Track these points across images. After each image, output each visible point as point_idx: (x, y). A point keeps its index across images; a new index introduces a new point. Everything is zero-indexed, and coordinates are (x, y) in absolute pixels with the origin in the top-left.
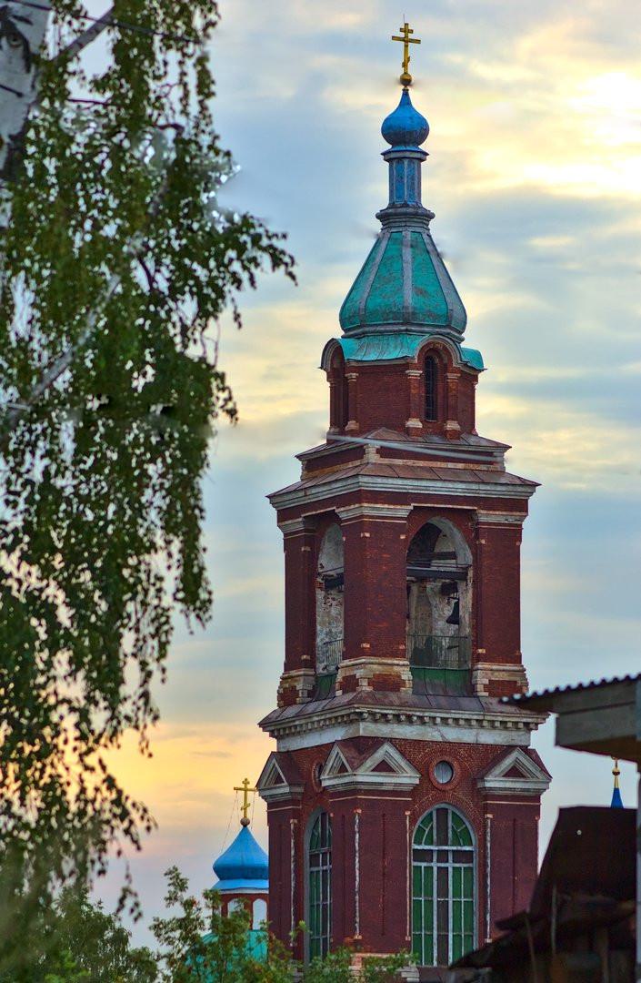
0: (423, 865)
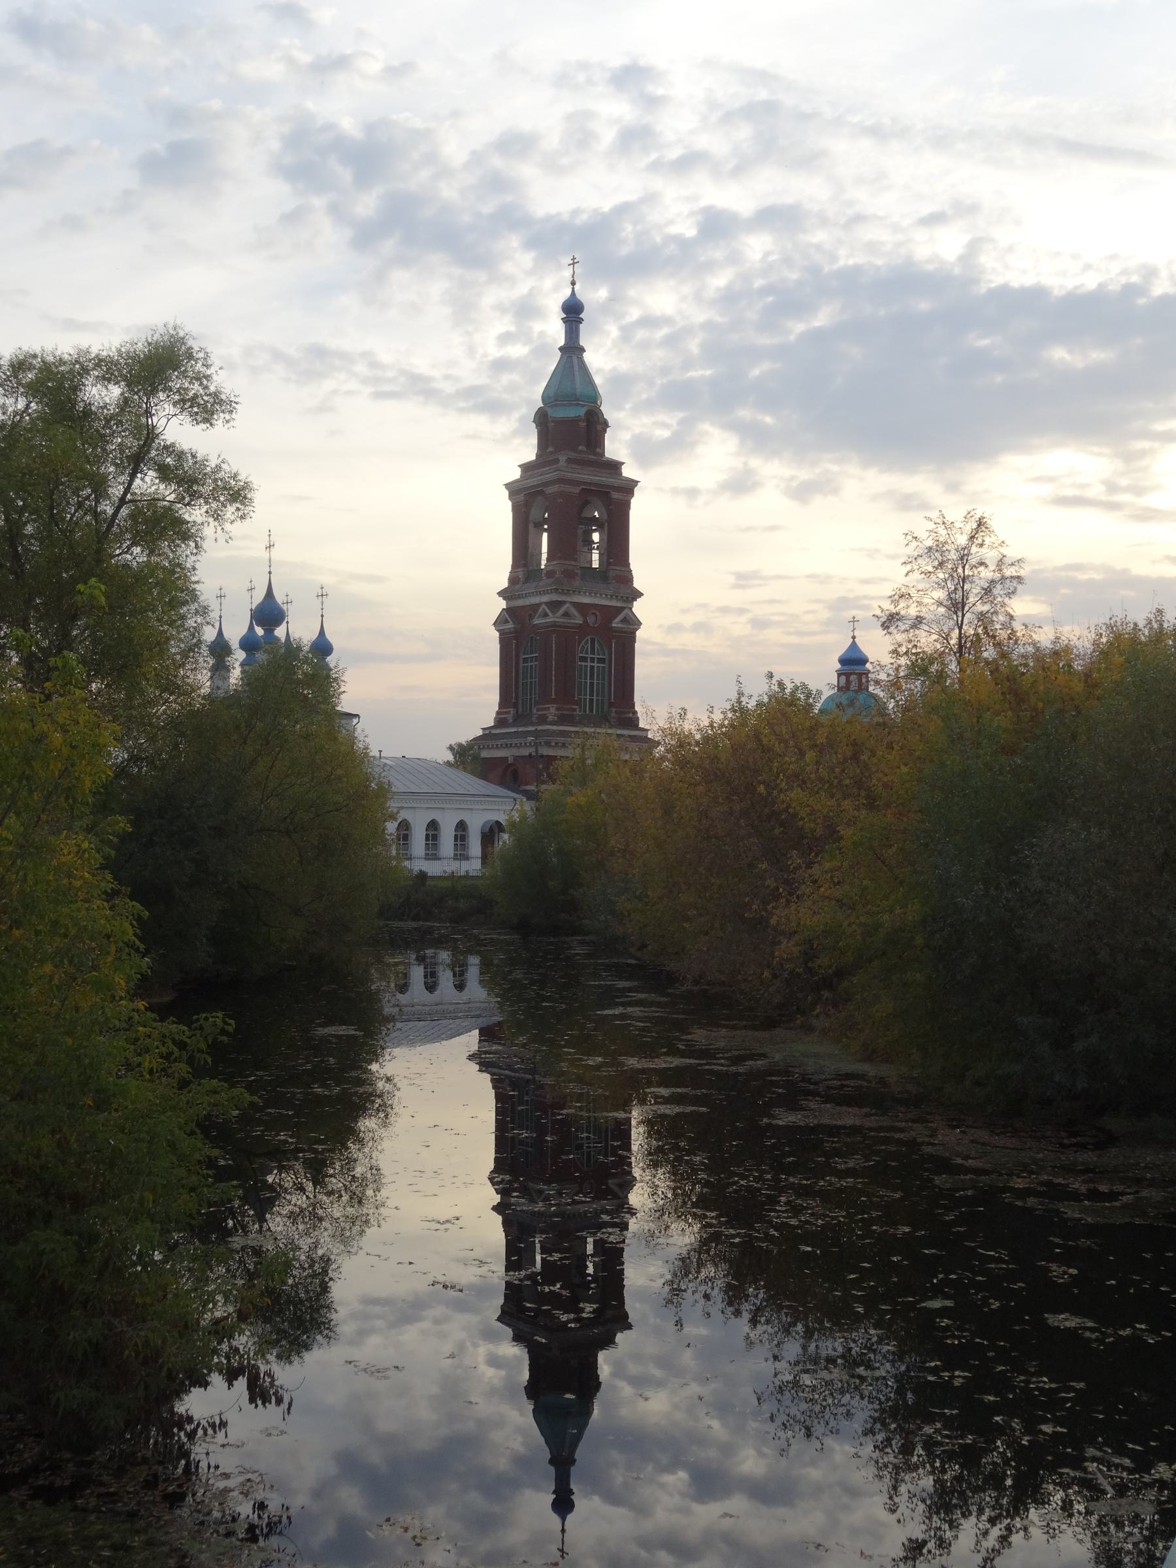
0: (583, 664)
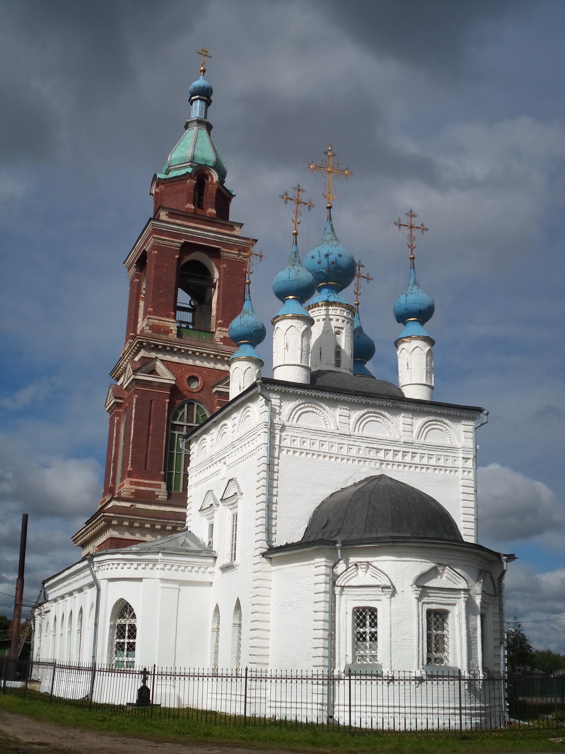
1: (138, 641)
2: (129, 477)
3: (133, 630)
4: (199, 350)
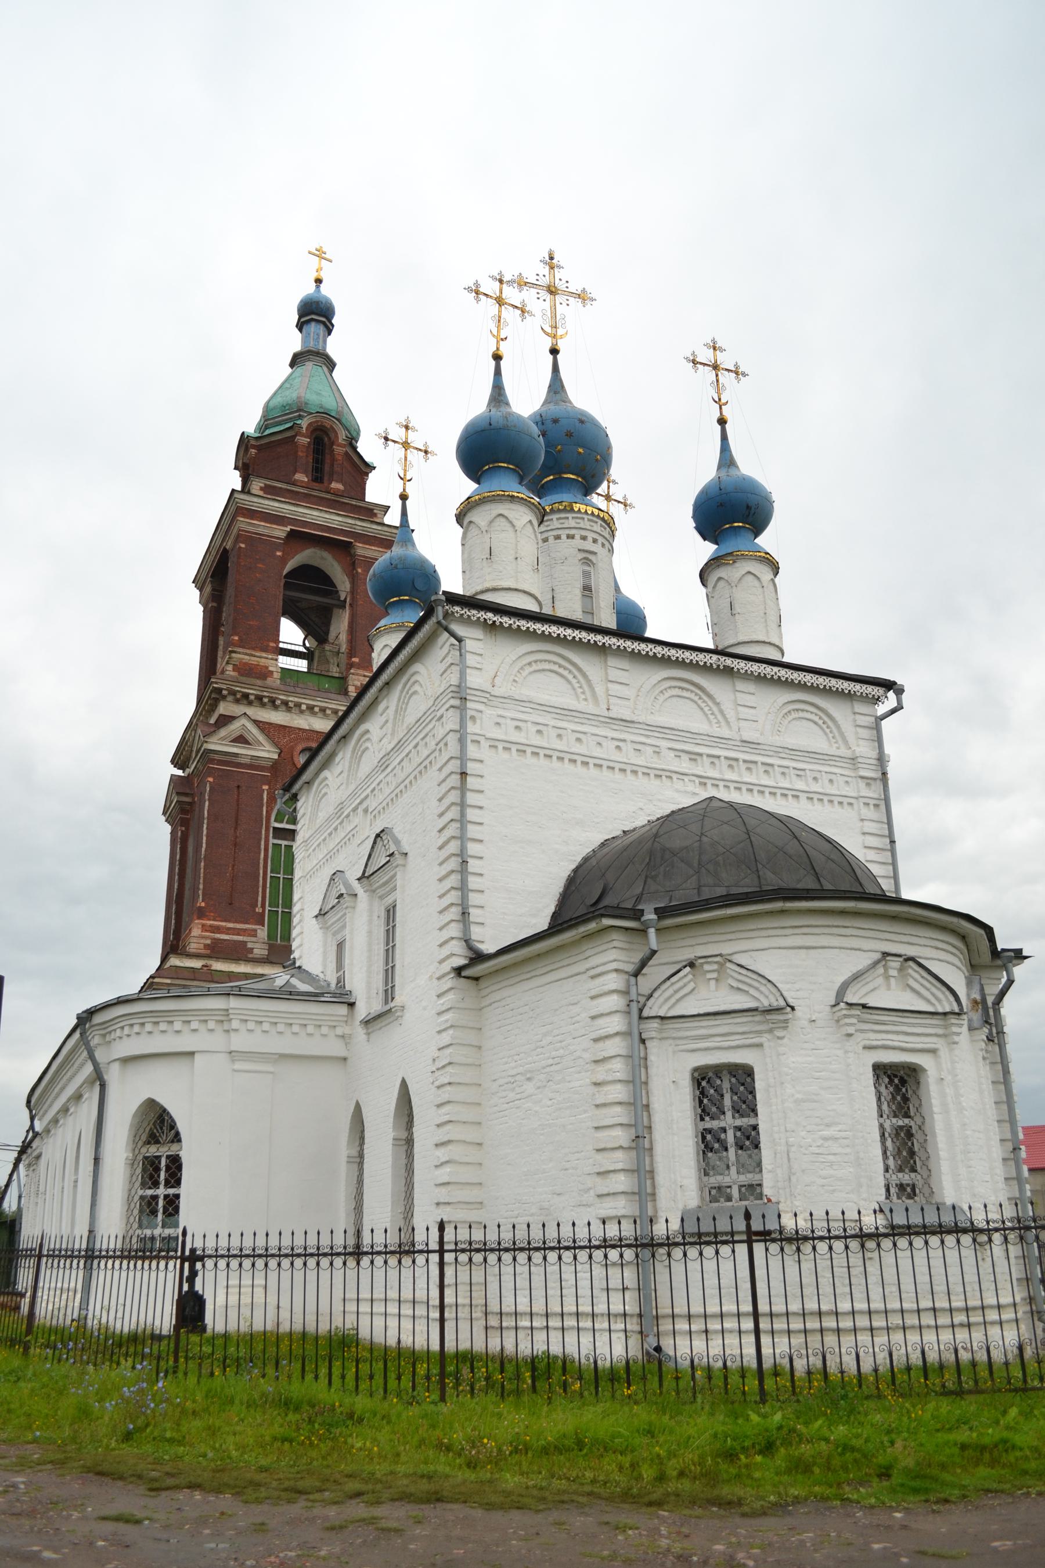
0: (284, 843)
1: (186, 1191)
2: (199, 918)
3: (175, 1165)
4: (319, 704)
